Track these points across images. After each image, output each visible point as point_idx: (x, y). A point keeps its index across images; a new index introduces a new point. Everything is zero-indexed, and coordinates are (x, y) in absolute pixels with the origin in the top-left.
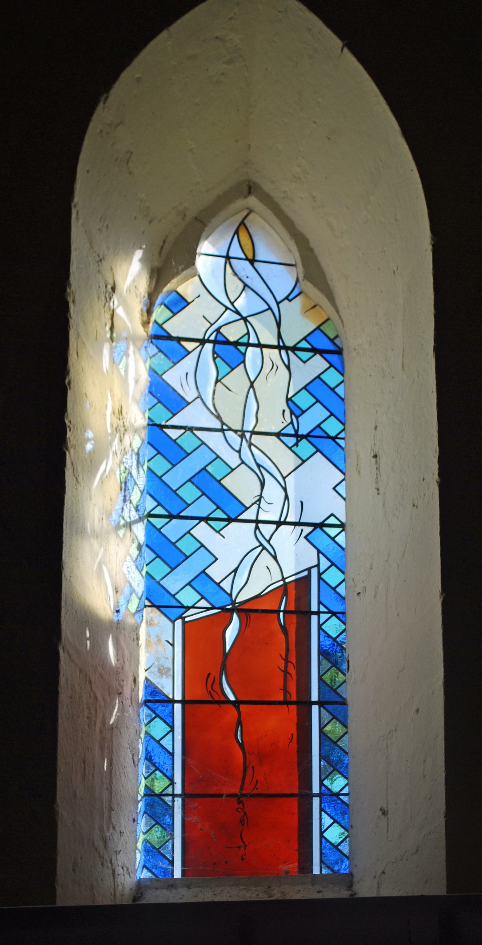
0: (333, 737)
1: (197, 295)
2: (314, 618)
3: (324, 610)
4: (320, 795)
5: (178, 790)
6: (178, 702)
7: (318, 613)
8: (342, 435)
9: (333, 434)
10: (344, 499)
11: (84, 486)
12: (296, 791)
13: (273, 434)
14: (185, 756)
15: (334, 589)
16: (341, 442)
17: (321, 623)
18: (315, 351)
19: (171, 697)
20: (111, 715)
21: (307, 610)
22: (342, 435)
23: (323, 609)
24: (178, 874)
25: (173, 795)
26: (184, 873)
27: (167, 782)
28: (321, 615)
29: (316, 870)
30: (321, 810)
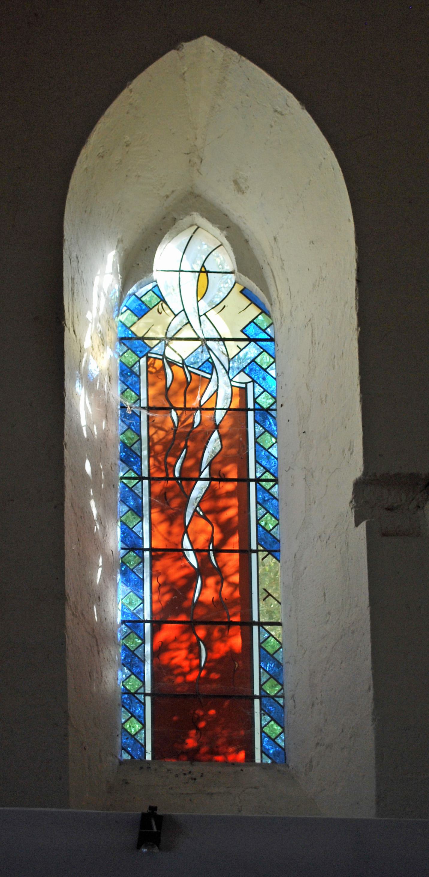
0: (271, 651)
1: (158, 272)
2: (254, 556)
3: (261, 548)
4: (260, 697)
5: (148, 690)
6: (147, 621)
7: (257, 551)
8: (274, 407)
9: (265, 406)
10: (275, 379)
11: (73, 279)
12: (237, 548)
13: (217, 339)
14: (151, 497)
15: (265, 390)
16: (273, 413)
17: (255, 397)
18: (249, 340)
19: (142, 618)
20: (97, 578)
21: (246, 477)
22: (274, 407)
23: (260, 548)
24: (149, 757)
25: (145, 695)
26: (153, 757)
27: (141, 684)
28: (260, 553)
29: (258, 760)
30: (255, 421)
